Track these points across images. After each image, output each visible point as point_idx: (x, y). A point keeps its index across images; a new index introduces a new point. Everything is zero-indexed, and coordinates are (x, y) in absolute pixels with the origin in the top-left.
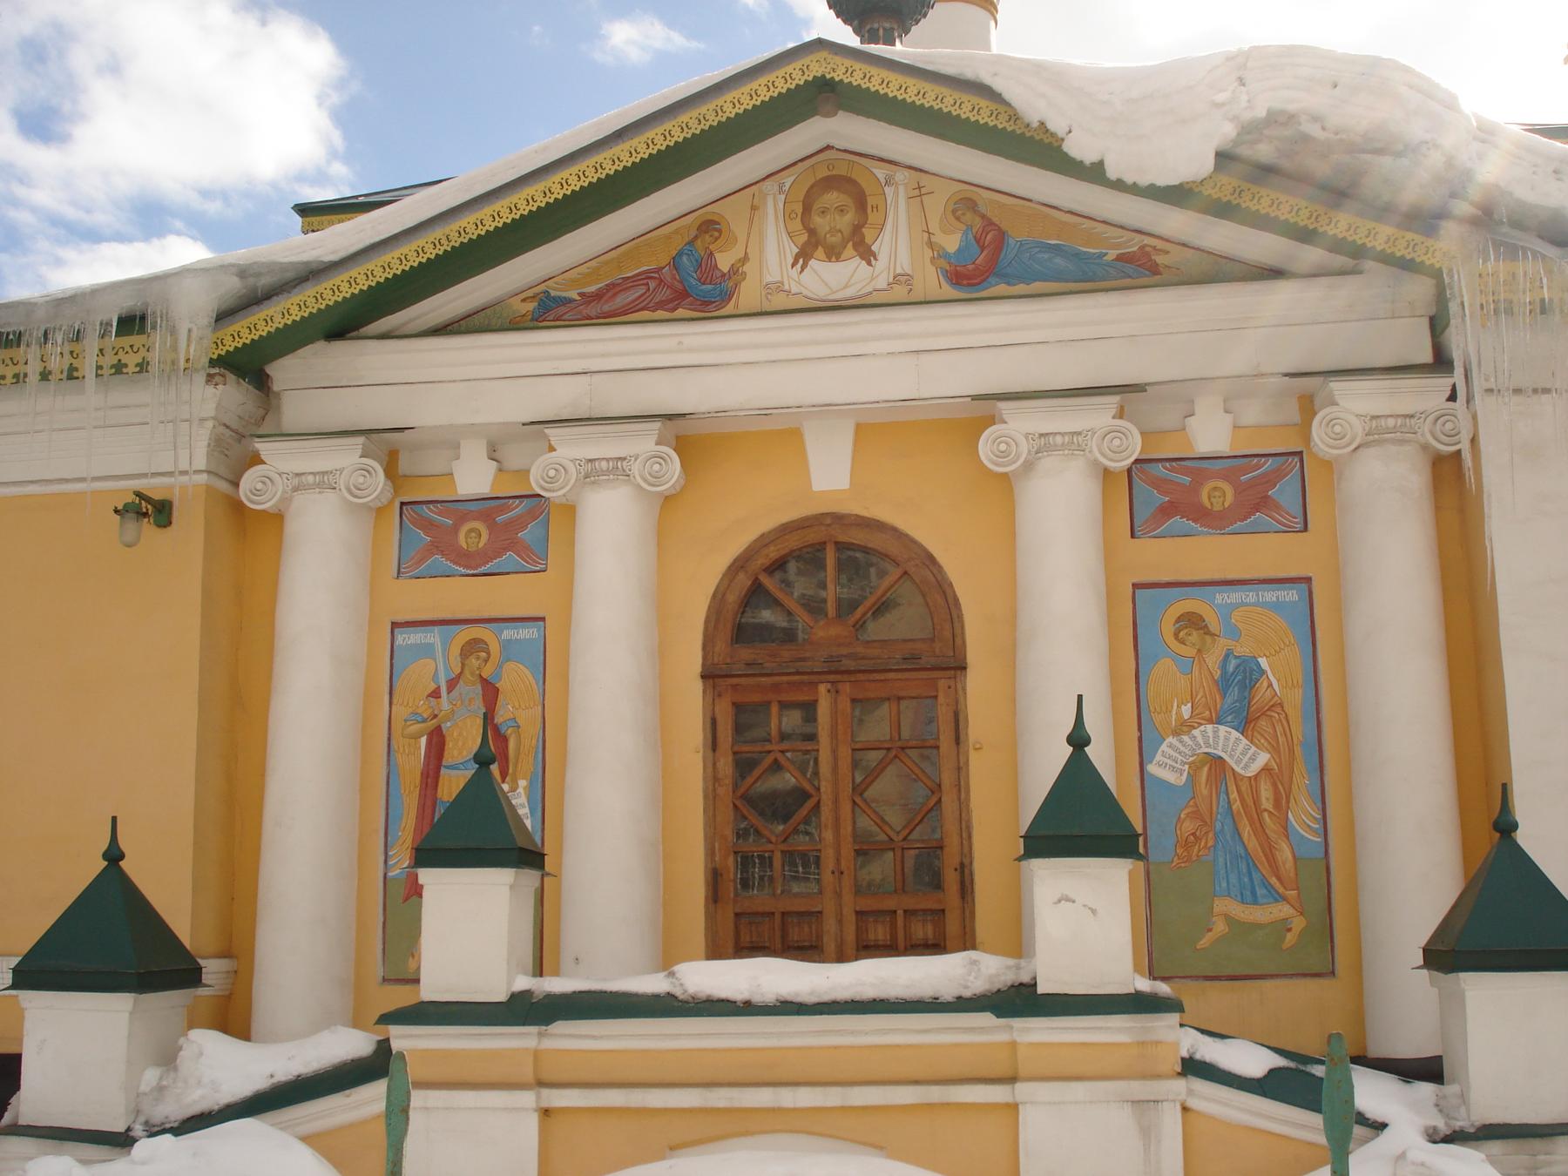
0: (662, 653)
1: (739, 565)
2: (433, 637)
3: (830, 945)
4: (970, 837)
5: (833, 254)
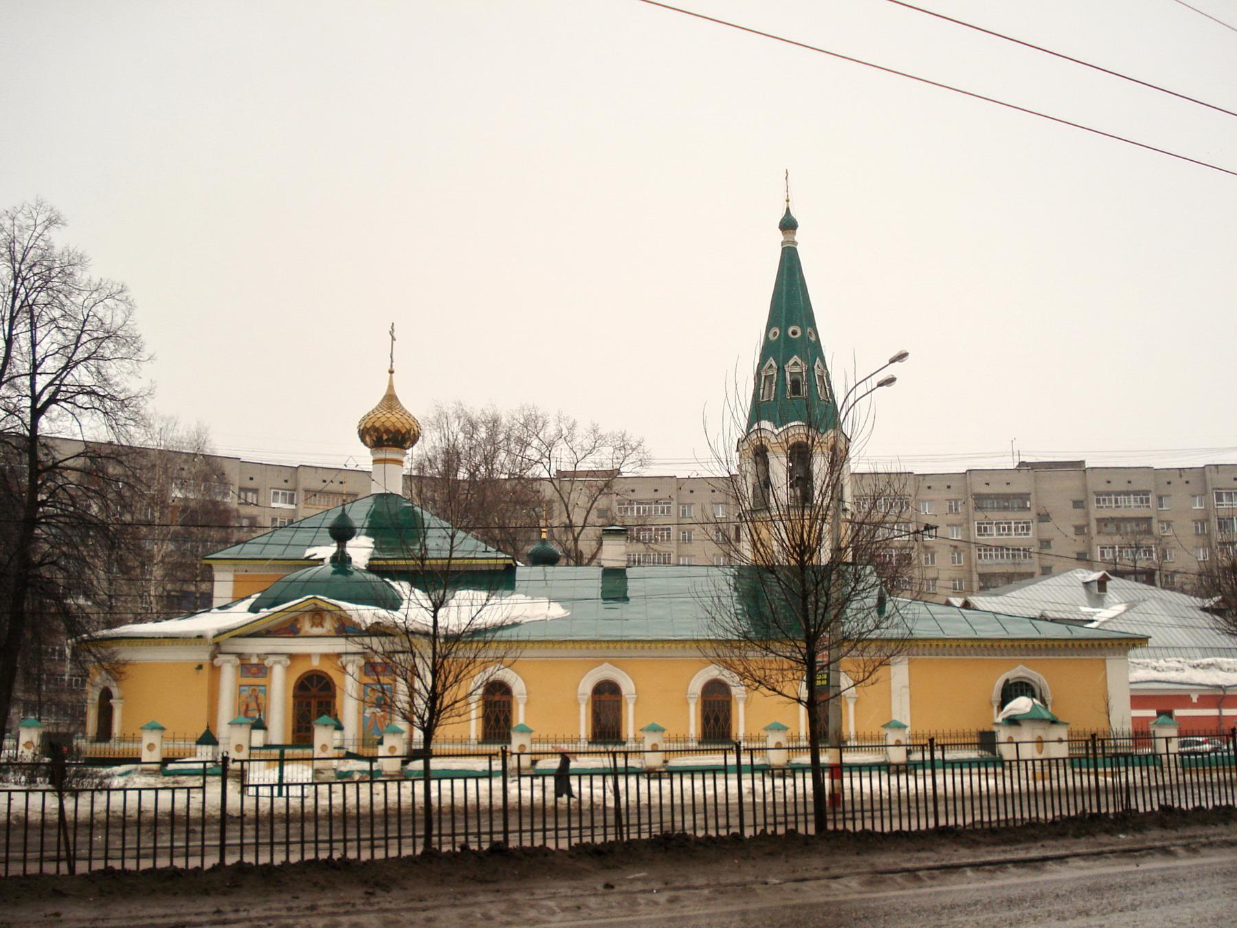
1: (299, 678)
2: (246, 688)
3: (491, 698)
4: (829, 382)
5: (317, 626)
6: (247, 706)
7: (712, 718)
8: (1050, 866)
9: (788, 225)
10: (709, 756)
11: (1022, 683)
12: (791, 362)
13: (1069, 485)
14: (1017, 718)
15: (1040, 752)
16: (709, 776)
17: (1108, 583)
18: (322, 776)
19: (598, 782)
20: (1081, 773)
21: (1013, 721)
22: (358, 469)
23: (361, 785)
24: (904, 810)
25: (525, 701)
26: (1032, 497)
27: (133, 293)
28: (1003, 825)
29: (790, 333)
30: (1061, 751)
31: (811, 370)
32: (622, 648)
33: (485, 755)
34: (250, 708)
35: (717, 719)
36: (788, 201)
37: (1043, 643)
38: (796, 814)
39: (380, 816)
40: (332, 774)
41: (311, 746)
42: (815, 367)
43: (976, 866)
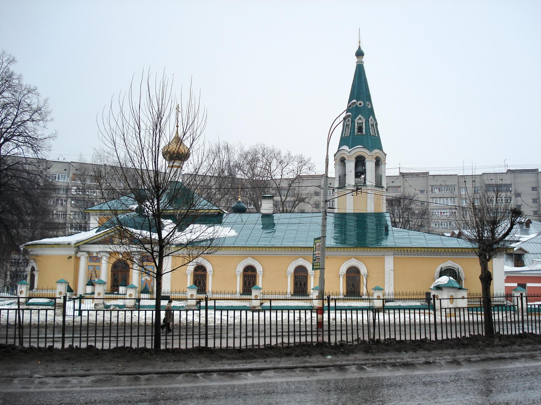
0: (108, 269)
6: (91, 275)
7: (299, 283)
8: (243, 375)
9: (360, 54)
10: (300, 302)
11: (450, 269)
12: (358, 118)
13: (530, 179)
14: (440, 286)
15: (452, 303)
16: (303, 312)
17: (531, 225)
18: (98, 307)
19: (190, 313)
20: (477, 314)
21: (439, 288)
22: (65, 161)
23: (112, 312)
24: (237, 334)
25: (212, 274)
26: (513, 186)
27: (39, 90)
28: (355, 343)
29: (358, 104)
30: (464, 303)
31: (367, 121)
32: (272, 250)
33: (268, 299)
34: (93, 276)
35: (301, 285)
36: (360, 43)
37: (460, 250)
38: (289, 332)
39: (85, 327)
40: (102, 306)
41: (251, 294)
42: (370, 120)
43: (219, 372)
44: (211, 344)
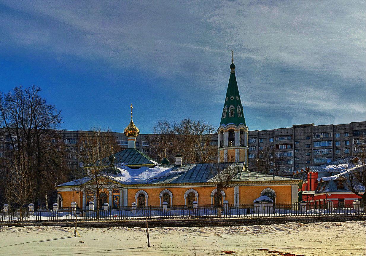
9: (233, 66)
12: (231, 107)
44: (70, 218)
